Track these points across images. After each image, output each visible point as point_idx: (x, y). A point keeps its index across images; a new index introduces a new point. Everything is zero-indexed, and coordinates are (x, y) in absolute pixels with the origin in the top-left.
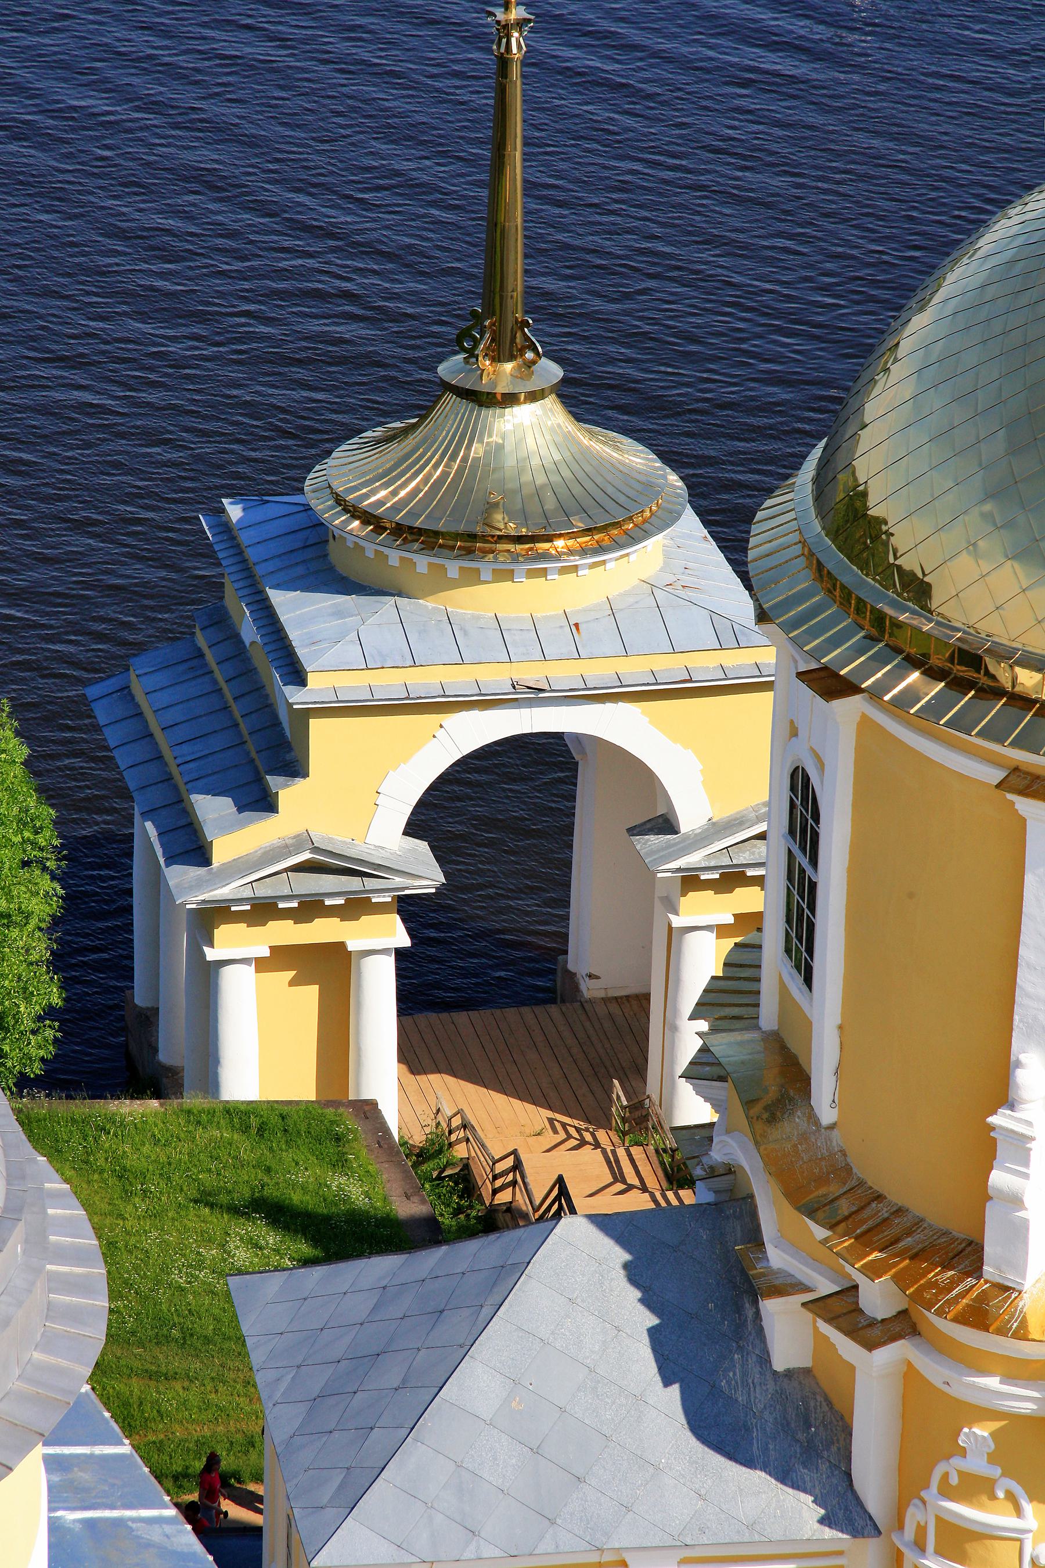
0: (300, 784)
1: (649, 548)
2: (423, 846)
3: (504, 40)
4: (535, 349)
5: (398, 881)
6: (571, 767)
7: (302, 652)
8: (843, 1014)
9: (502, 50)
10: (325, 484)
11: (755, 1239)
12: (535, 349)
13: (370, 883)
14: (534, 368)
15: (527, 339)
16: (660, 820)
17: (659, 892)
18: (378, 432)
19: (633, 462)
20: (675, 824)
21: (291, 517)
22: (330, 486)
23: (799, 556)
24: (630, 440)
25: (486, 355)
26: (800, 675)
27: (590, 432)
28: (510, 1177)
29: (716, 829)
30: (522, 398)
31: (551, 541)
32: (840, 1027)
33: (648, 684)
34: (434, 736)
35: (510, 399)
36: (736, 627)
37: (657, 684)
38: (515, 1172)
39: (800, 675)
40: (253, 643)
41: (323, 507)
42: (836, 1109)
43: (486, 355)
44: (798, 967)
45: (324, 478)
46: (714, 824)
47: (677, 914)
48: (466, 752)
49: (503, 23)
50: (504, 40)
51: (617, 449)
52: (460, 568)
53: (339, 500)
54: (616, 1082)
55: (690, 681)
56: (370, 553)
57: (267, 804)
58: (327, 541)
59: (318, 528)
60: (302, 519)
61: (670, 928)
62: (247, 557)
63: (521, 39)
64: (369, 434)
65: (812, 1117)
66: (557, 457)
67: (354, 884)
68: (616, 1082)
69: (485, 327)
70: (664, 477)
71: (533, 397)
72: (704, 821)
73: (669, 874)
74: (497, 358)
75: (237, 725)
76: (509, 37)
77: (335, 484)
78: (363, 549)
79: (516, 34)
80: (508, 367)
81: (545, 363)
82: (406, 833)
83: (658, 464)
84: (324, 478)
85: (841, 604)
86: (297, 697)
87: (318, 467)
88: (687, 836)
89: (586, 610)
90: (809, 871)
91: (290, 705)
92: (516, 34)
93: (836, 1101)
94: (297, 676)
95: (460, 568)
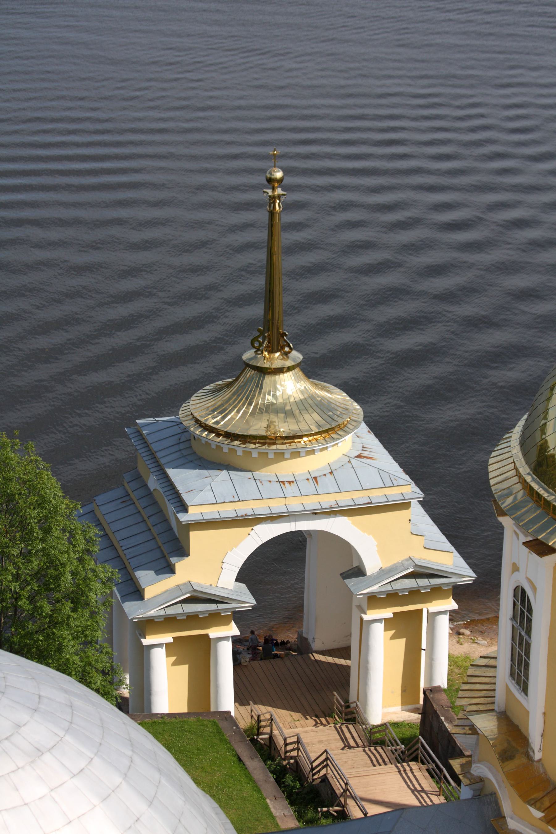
0: (186, 560)
1: (347, 440)
2: (243, 586)
3: (272, 205)
4: (289, 346)
5: (233, 605)
6: (305, 540)
7: (186, 497)
8: (545, 707)
9: (272, 209)
10: (190, 413)
11: (501, 817)
12: (289, 346)
13: (221, 606)
14: (289, 355)
15: (285, 341)
16: (356, 569)
17: (355, 603)
18: (211, 386)
19: (336, 397)
20: (364, 571)
21: (171, 429)
22: (192, 414)
23: (517, 483)
24: (339, 390)
25: (266, 350)
26: (524, 543)
27: (316, 384)
28: (325, 763)
29: (383, 573)
30: (285, 370)
31: (302, 438)
32: (544, 714)
33: (351, 506)
34: (249, 534)
35: (280, 371)
36: (391, 476)
37: (355, 505)
38: (327, 761)
39: (524, 543)
40: (155, 490)
41: (188, 423)
42: (541, 753)
43: (266, 350)
44: (518, 683)
45: (189, 410)
46: (383, 570)
47: (365, 613)
48: (265, 541)
49: (272, 197)
50: (272, 205)
51: (328, 391)
52: (258, 452)
53: (197, 421)
54: (335, 693)
55: (371, 503)
56: (226, 450)
57: (171, 570)
58: (190, 440)
59: (185, 434)
60: (177, 430)
61: (362, 619)
62: (151, 448)
63: (280, 204)
64: (207, 387)
65: (529, 758)
66: (302, 397)
67: (213, 607)
68: (335, 693)
69: (265, 337)
70: (352, 404)
71: (289, 369)
72: (377, 570)
73: (362, 596)
74: (272, 351)
75: (150, 529)
76: (274, 203)
77: (195, 415)
78: (210, 444)
79: (278, 201)
80: (277, 354)
81: (294, 353)
82: (237, 580)
83: (348, 398)
84: (189, 410)
85: (544, 508)
86: (183, 518)
87: (184, 405)
88: (370, 576)
89: (318, 470)
90: (526, 637)
91: (181, 522)
92: (278, 201)
93: (541, 749)
94: (184, 508)
95: (258, 452)
